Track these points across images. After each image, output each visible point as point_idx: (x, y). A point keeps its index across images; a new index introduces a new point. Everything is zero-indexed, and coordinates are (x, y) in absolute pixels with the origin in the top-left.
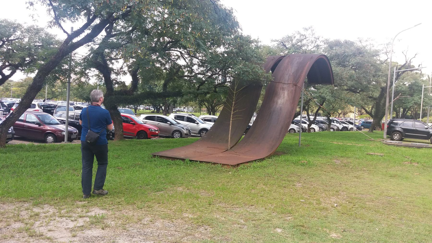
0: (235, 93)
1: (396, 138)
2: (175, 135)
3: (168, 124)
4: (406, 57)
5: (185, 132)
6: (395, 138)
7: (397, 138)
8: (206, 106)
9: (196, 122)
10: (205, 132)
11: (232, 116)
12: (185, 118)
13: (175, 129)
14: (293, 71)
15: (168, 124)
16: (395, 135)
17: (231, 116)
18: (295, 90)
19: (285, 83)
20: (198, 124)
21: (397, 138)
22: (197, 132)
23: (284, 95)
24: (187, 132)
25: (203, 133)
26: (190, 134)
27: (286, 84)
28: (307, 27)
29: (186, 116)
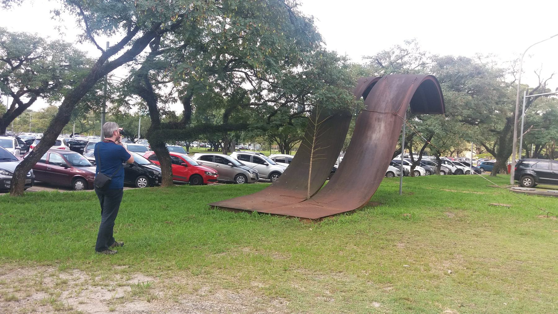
0: (316, 125)
1: (527, 184)
2: (238, 180)
3: (229, 165)
4: (539, 78)
5: (251, 175)
6: (526, 183)
7: (528, 184)
8: (278, 143)
9: (265, 163)
10: (277, 176)
11: (312, 155)
12: (251, 158)
13: (238, 172)
14: (392, 96)
15: (229, 165)
16: (525, 180)
17: (311, 156)
18: (395, 122)
19: (382, 112)
20: (267, 165)
21: (528, 184)
22: (266, 176)
23: (380, 128)
24: (253, 176)
25: (274, 177)
26: (258, 178)
27: (382, 113)
28: (410, 40)
29: (253, 155)
